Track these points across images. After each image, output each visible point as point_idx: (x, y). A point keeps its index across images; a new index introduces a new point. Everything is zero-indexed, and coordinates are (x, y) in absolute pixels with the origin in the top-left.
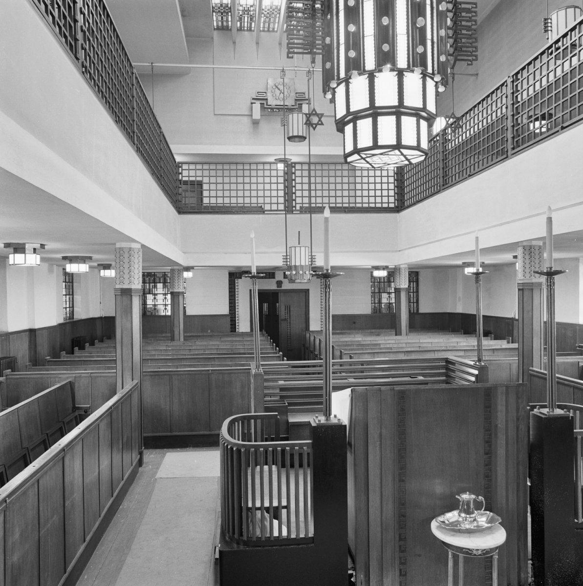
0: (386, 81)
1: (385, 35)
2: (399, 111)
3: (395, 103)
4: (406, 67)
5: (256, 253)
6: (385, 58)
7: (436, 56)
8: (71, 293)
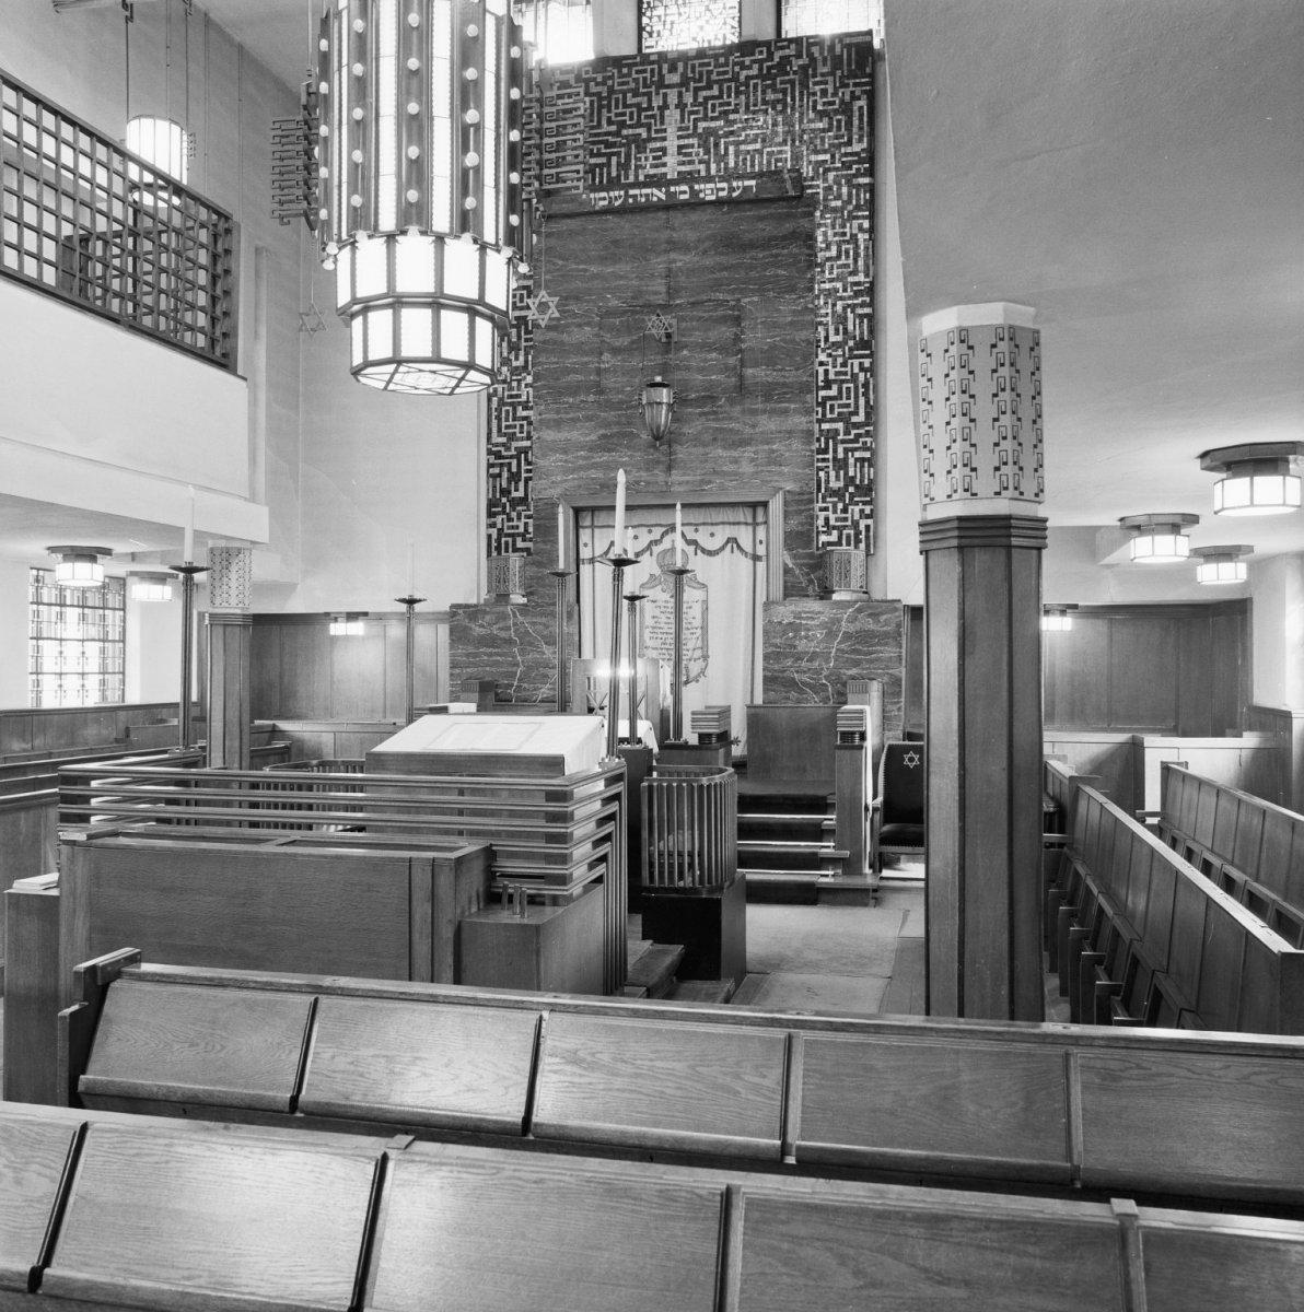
0: (414, 247)
1: (417, 173)
2: (437, 302)
3: (430, 288)
4: (447, 231)
5: (790, 1038)
6: (414, 214)
7: (503, 89)
8: (114, 634)
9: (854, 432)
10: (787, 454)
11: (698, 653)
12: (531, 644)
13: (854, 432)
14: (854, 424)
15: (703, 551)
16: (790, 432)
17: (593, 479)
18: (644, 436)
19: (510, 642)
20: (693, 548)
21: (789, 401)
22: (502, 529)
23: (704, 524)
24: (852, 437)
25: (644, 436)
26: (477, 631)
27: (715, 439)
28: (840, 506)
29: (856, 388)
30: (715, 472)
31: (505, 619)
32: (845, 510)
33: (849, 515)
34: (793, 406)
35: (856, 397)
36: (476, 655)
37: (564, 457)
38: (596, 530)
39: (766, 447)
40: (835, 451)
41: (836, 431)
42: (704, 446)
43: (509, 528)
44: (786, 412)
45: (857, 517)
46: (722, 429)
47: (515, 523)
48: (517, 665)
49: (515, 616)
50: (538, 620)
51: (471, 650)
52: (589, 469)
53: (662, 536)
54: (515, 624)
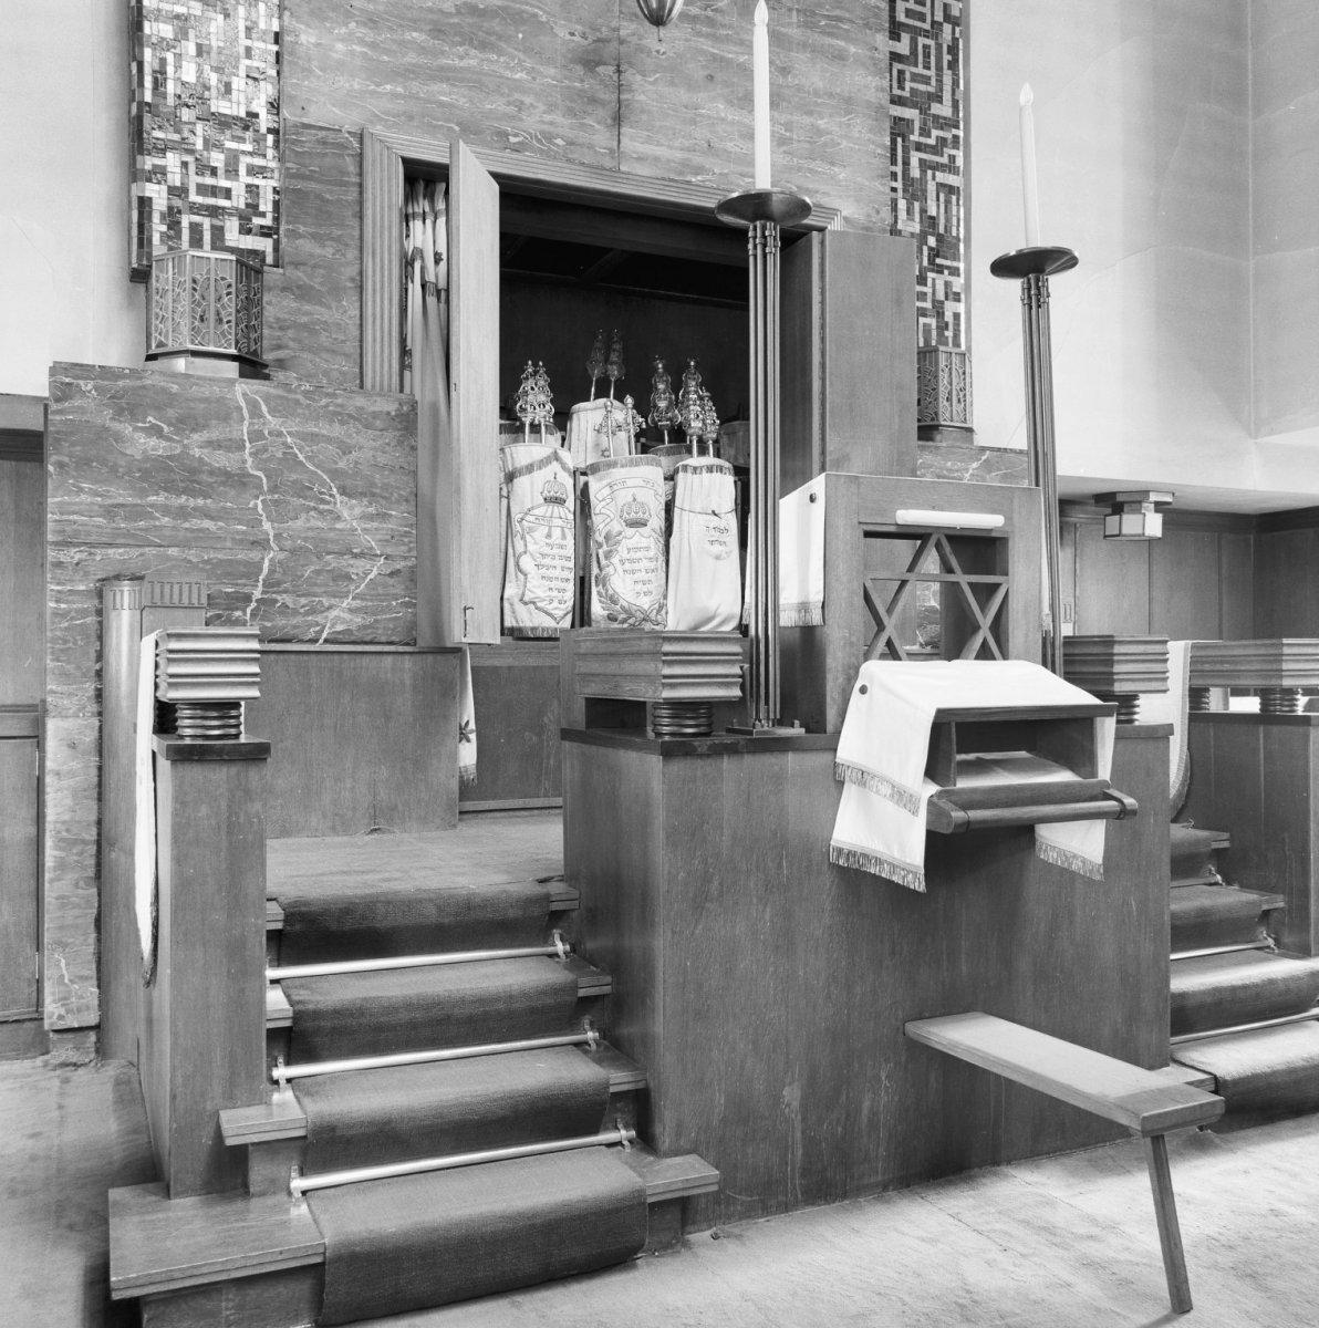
12: (302, 490)
14: (937, 117)
16: (849, 101)
18: (562, 33)
19: (240, 481)
21: (847, 38)
24: (932, 141)
25: (562, 33)
27: (711, 78)
29: (939, 47)
33: (928, 290)
34: (853, 49)
35: (939, 69)
36: (137, 513)
37: (370, 36)
39: (807, 120)
40: (906, 163)
41: (909, 123)
42: (691, 86)
43: (202, 190)
44: (840, 57)
46: (722, 59)
49: (255, 412)
50: (323, 429)
51: (121, 495)
52: (433, 78)
54: (256, 436)
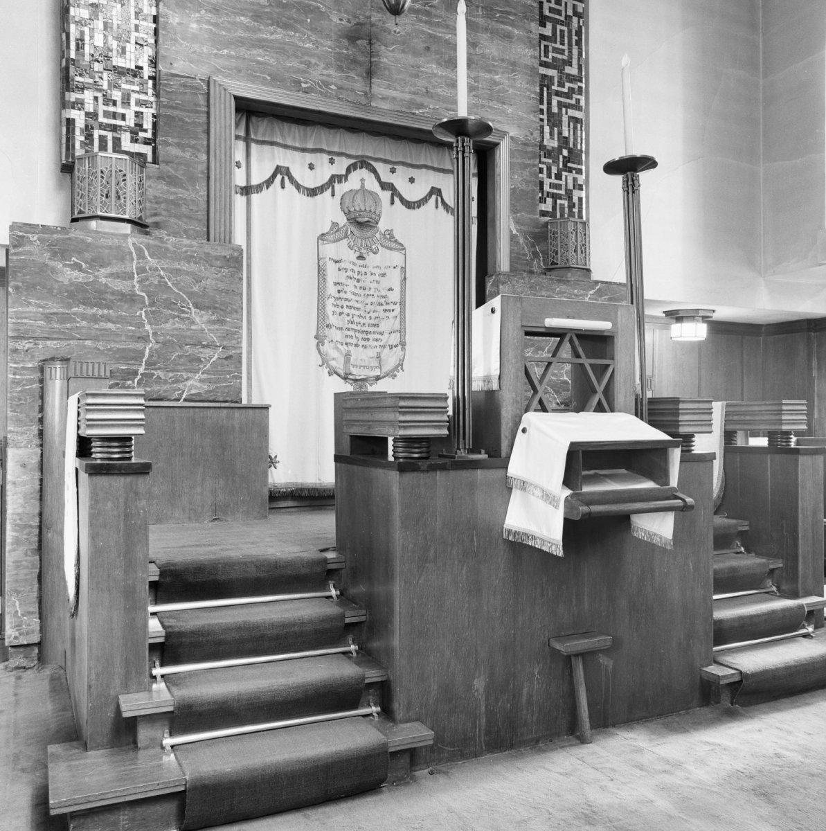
9: (567, 85)
10: (511, 91)
11: (395, 339)
12: (170, 305)
13: (567, 85)
14: (568, 75)
15: (403, 200)
16: (514, 64)
17: (259, 62)
19: (131, 299)
20: (388, 194)
21: (512, 24)
22: (94, 115)
23: (403, 164)
24: (565, 90)
25: (335, 19)
26: (68, 275)
27: (428, 49)
28: (554, 170)
29: (570, 31)
30: (427, 93)
31: (122, 259)
32: (558, 176)
34: (516, 32)
35: (570, 45)
36: (64, 318)
37: (214, 19)
38: (253, 146)
39: (488, 76)
40: (549, 103)
42: (416, 53)
45: (570, 186)
46: (435, 37)
47: (120, 110)
48: (144, 339)
49: (141, 256)
51: (55, 307)
53: (348, 170)
54: (141, 270)
